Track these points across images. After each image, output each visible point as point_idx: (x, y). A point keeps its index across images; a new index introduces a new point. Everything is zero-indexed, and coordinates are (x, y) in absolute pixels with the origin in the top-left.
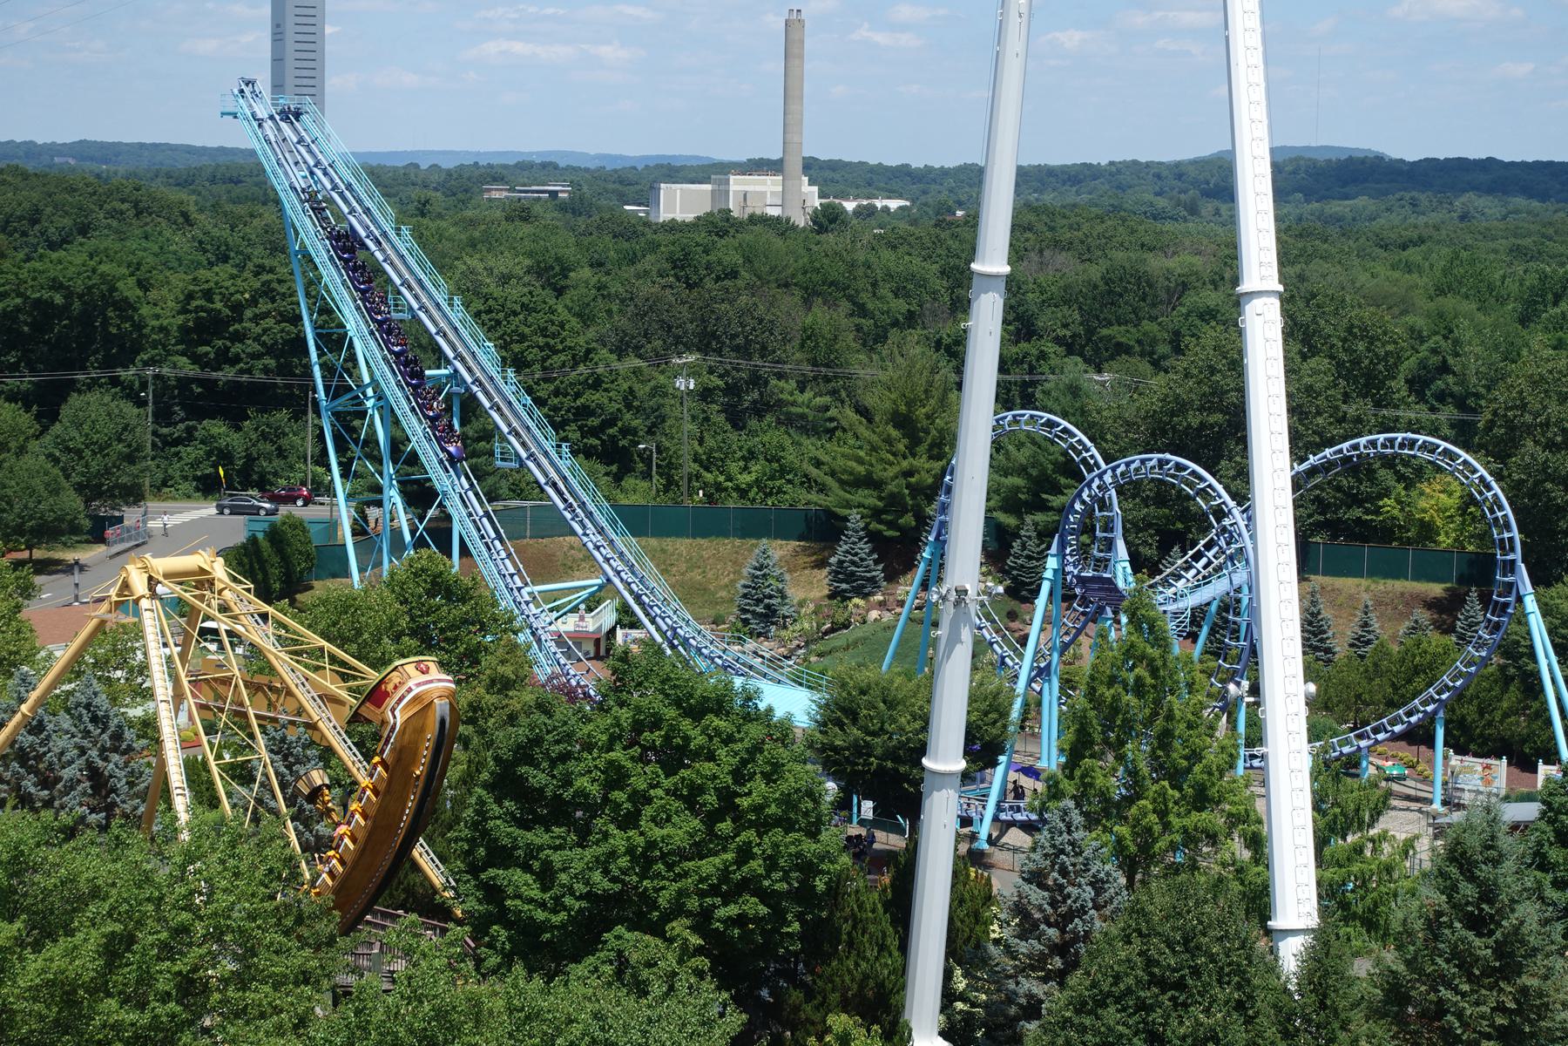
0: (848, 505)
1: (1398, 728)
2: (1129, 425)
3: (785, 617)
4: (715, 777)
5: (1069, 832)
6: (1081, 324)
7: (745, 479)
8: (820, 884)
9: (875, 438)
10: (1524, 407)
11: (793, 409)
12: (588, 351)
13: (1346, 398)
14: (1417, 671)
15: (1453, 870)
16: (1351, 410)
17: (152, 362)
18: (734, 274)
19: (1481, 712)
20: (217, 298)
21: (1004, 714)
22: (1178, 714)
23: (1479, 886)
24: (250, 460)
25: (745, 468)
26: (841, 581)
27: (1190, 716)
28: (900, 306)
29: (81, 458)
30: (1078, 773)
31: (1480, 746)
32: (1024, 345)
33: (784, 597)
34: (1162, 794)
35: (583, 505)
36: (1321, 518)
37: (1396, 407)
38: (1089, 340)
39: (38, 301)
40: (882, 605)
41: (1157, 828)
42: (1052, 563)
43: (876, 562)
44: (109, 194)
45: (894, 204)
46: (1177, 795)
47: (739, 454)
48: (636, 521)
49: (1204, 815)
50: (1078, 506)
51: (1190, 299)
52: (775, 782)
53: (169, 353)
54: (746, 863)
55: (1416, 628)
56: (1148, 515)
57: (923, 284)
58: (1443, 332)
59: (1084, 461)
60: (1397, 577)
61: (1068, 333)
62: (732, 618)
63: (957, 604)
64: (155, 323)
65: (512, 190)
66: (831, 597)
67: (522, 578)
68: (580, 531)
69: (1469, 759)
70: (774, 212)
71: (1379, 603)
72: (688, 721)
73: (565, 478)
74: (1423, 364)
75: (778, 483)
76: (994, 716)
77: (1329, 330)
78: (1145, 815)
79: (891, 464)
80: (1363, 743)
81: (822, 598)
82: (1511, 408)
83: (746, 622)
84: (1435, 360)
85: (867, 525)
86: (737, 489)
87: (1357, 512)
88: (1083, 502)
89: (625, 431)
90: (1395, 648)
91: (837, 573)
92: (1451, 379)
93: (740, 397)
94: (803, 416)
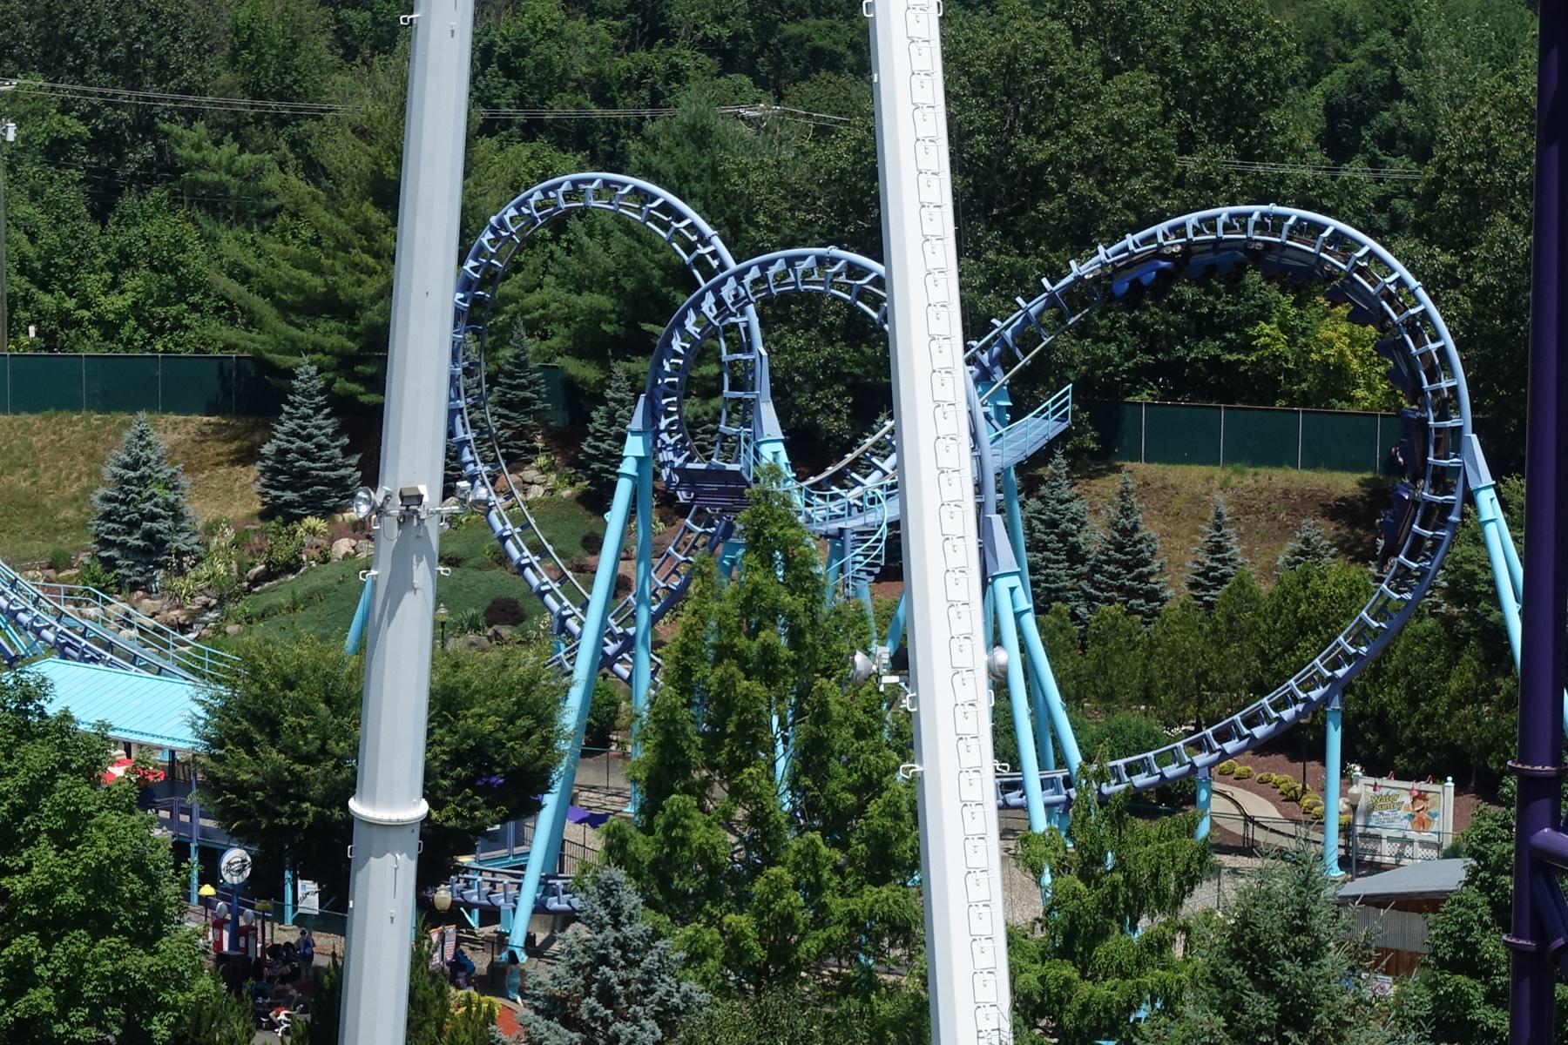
0: (295, 349)
1: (1260, 731)
2: (797, 197)
3: (180, 554)
5: (617, 925)
6: (748, 16)
7: (115, 303)
9: (339, 225)
10: (1492, 155)
13: (1187, 144)
14: (1303, 627)
15: (1236, 972)
16: (1192, 164)
19: (1413, 700)
21: (544, 718)
22: (835, 708)
23: (1281, 999)
25: (114, 286)
26: (283, 487)
27: (859, 714)
30: (660, 821)
31: (1411, 758)
33: (178, 516)
34: (810, 854)
36: (1149, 359)
37: (1280, 159)
38: (765, 45)
41: (804, 917)
42: (634, 447)
43: (347, 451)
46: (838, 856)
47: (101, 259)
49: (885, 891)
50: (677, 344)
52: (73, 846)
54: (23, 993)
55: (1308, 551)
56: (834, 358)
58: (1392, 23)
59: (701, 262)
60: (1277, 463)
61: (726, 33)
62: (84, 558)
63: (404, 520)
66: (266, 516)
69: (1389, 783)
71: (1244, 508)
74: (1355, 84)
75: (173, 310)
76: (525, 722)
77: (1158, 21)
78: (779, 894)
79: (371, 272)
80: (1201, 759)
81: (249, 518)
82: (1469, 158)
83: (109, 564)
84: (1379, 74)
85: (330, 383)
86: (99, 321)
87: (1213, 348)
88: (686, 336)
90: (1265, 588)
91: (275, 472)
92: (1402, 106)
93: (120, 156)
94: (221, 187)
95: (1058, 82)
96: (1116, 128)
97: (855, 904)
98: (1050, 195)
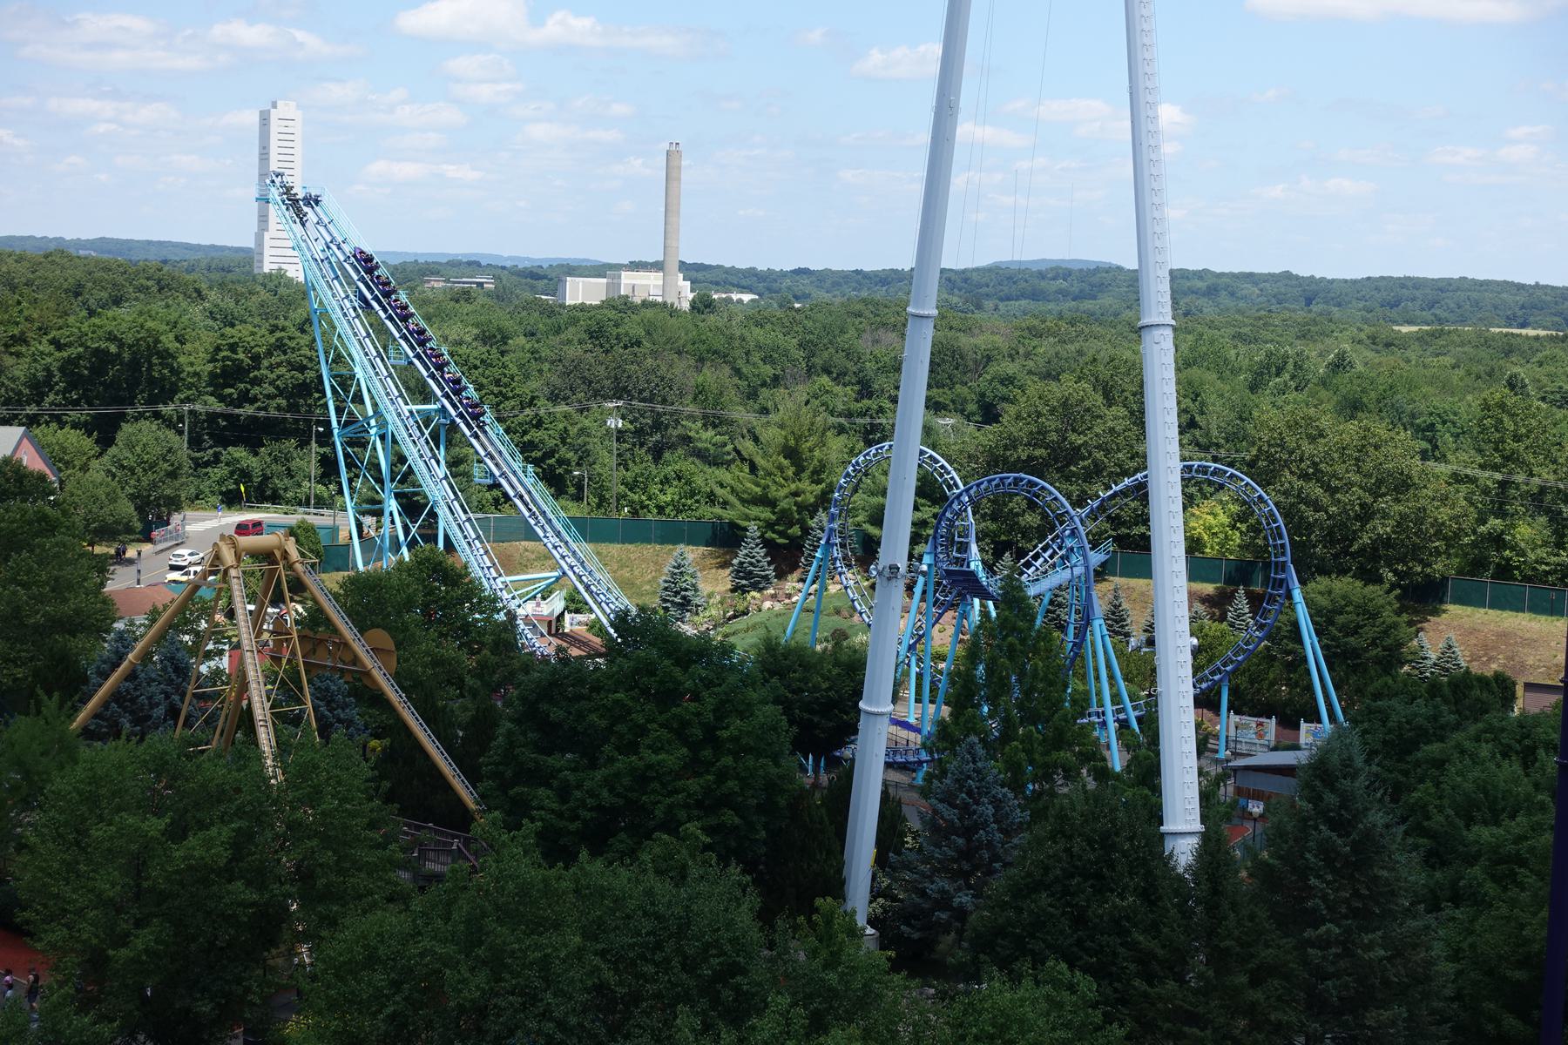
0: (747, 518)
4: (698, 714)
5: (974, 762)
8: (782, 802)
10: (1282, 446)
11: (699, 445)
12: (533, 398)
17: (188, 400)
18: (639, 344)
19: (1252, 682)
20: (240, 350)
24: (266, 478)
28: (768, 370)
29: (133, 474)
30: (962, 720)
32: (866, 402)
33: (696, 590)
35: (543, 513)
39: (97, 349)
40: (774, 597)
43: (769, 564)
44: (137, 273)
45: (747, 298)
48: (588, 530)
51: (993, 369)
53: (200, 394)
57: (786, 353)
64: (191, 369)
65: (448, 281)
66: (733, 591)
67: (497, 571)
68: (541, 534)
70: (660, 299)
72: (678, 669)
73: (529, 492)
89: (561, 462)
94: (707, 449)
95: (1088, 410)
96: (1112, 430)
97: (1047, 759)
98: (1084, 459)
